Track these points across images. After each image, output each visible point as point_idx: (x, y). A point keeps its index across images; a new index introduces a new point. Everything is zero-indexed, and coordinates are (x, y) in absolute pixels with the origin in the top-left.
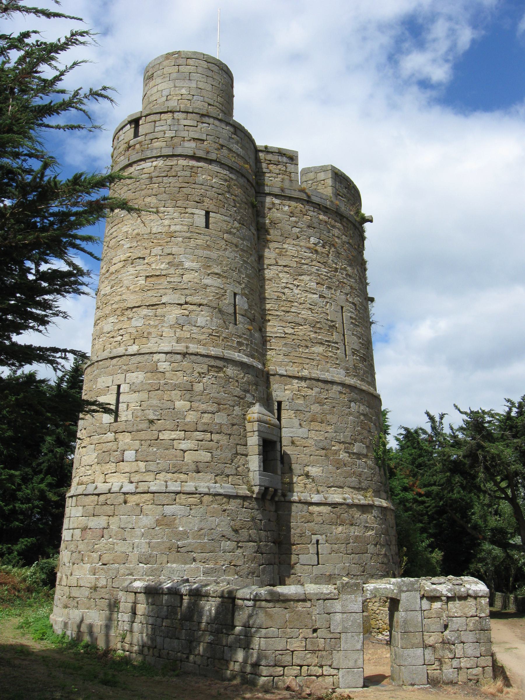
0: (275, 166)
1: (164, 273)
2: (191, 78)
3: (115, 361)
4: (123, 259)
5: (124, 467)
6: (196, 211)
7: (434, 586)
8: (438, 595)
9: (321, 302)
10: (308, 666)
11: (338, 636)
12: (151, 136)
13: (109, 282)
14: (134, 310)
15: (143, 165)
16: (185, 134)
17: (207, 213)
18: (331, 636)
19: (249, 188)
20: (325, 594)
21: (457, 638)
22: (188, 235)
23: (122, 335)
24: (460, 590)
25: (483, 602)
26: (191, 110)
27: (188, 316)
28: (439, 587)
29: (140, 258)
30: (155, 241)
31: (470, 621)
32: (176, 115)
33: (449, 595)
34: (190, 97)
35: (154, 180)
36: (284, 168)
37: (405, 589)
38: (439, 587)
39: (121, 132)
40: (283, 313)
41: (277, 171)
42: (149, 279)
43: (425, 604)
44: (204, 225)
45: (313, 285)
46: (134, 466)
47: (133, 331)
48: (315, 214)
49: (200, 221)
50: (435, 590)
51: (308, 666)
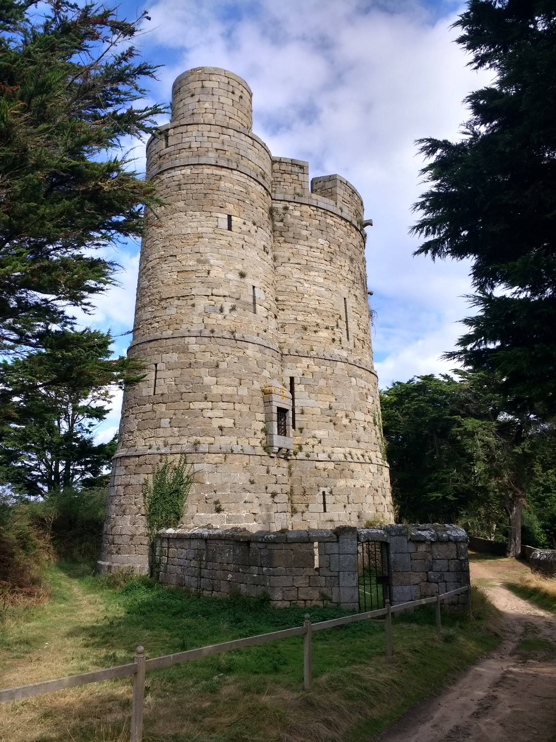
0: (288, 176)
1: (194, 269)
2: (214, 93)
3: (152, 344)
4: (157, 256)
5: (160, 432)
6: (219, 215)
7: (420, 532)
8: (422, 540)
9: (328, 294)
10: (311, 600)
11: (336, 574)
12: (179, 147)
13: (146, 277)
14: (168, 300)
15: (173, 173)
16: (208, 145)
17: (230, 217)
18: (330, 574)
19: (265, 195)
20: (325, 537)
21: (440, 578)
22: (213, 236)
23: (158, 322)
24: (442, 536)
25: (462, 546)
26: (213, 123)
27: (213, 306)
28: (424, 533)
29: (171, 256)
30: (184, 241)
31: (451, 563)
32: (200, 127)
33: (433, 540)
34: (214, 111)
35: (183, 187)
36: (296, 178)
37: (394, 534)
38: (424, 533)
39: (152, 144)
40: (295, 303)
41: (291, 181)
42: (180, 274)
43: (411, 548)
44: (226, 226)
45: (321, 280)
46: (169, 432)
47: (167, 318)
48: (323, 218)
49: (224, 224)
50: (420, 535)
51: (311, 600)
